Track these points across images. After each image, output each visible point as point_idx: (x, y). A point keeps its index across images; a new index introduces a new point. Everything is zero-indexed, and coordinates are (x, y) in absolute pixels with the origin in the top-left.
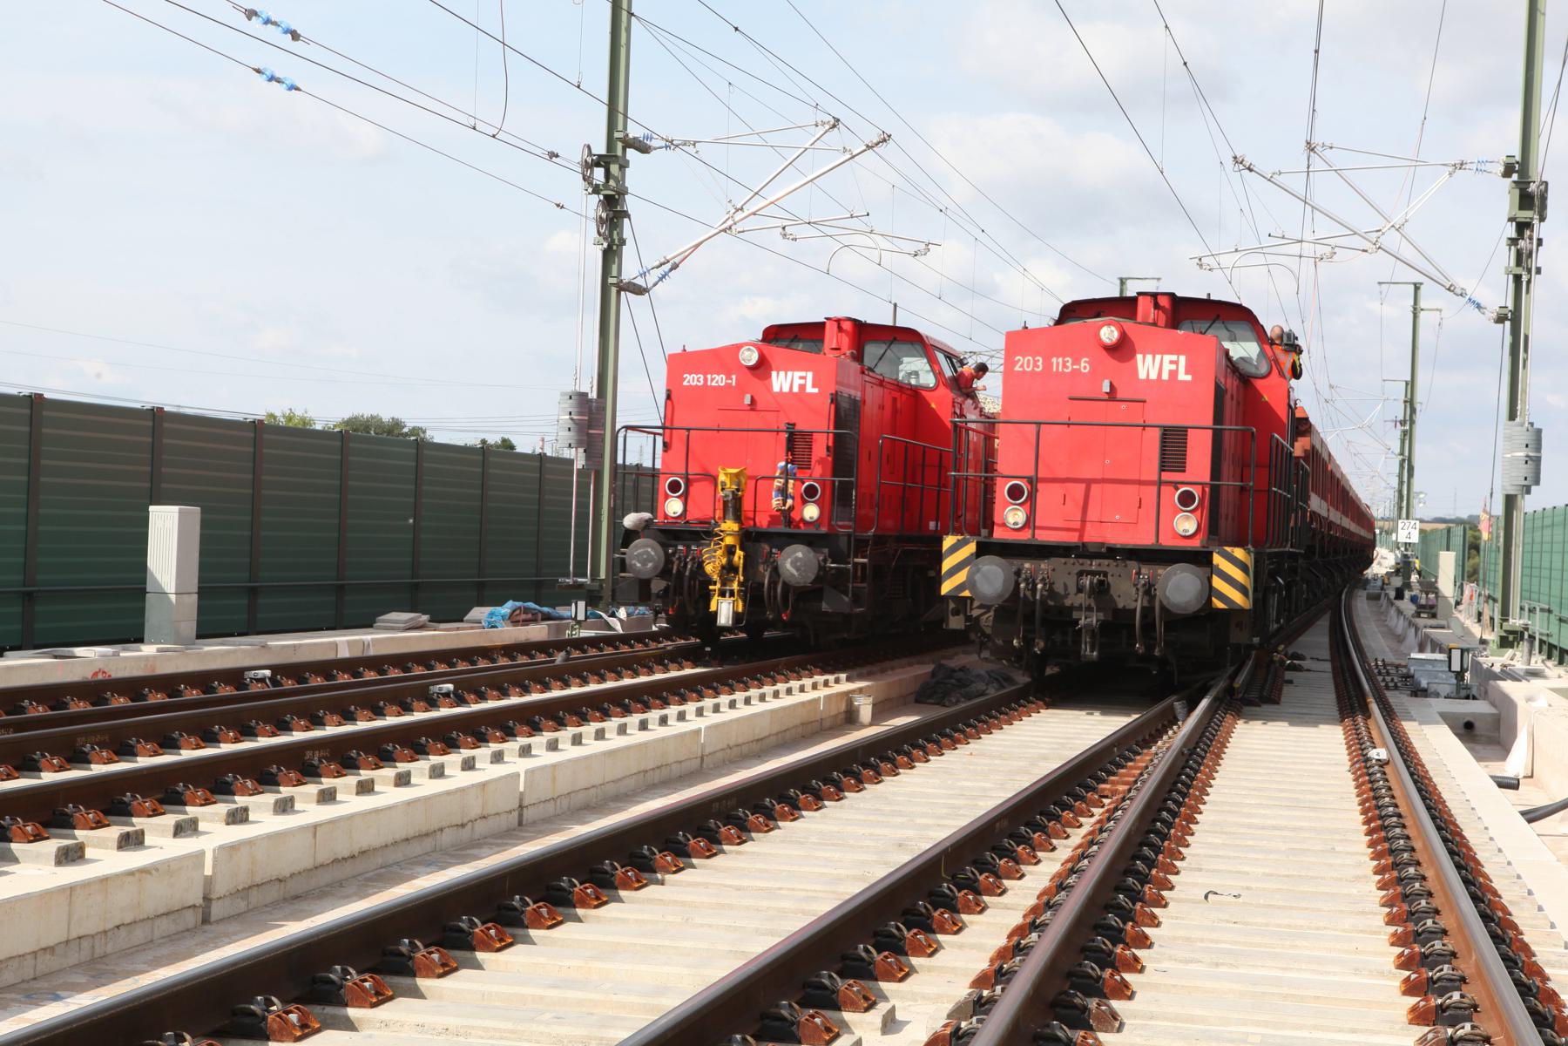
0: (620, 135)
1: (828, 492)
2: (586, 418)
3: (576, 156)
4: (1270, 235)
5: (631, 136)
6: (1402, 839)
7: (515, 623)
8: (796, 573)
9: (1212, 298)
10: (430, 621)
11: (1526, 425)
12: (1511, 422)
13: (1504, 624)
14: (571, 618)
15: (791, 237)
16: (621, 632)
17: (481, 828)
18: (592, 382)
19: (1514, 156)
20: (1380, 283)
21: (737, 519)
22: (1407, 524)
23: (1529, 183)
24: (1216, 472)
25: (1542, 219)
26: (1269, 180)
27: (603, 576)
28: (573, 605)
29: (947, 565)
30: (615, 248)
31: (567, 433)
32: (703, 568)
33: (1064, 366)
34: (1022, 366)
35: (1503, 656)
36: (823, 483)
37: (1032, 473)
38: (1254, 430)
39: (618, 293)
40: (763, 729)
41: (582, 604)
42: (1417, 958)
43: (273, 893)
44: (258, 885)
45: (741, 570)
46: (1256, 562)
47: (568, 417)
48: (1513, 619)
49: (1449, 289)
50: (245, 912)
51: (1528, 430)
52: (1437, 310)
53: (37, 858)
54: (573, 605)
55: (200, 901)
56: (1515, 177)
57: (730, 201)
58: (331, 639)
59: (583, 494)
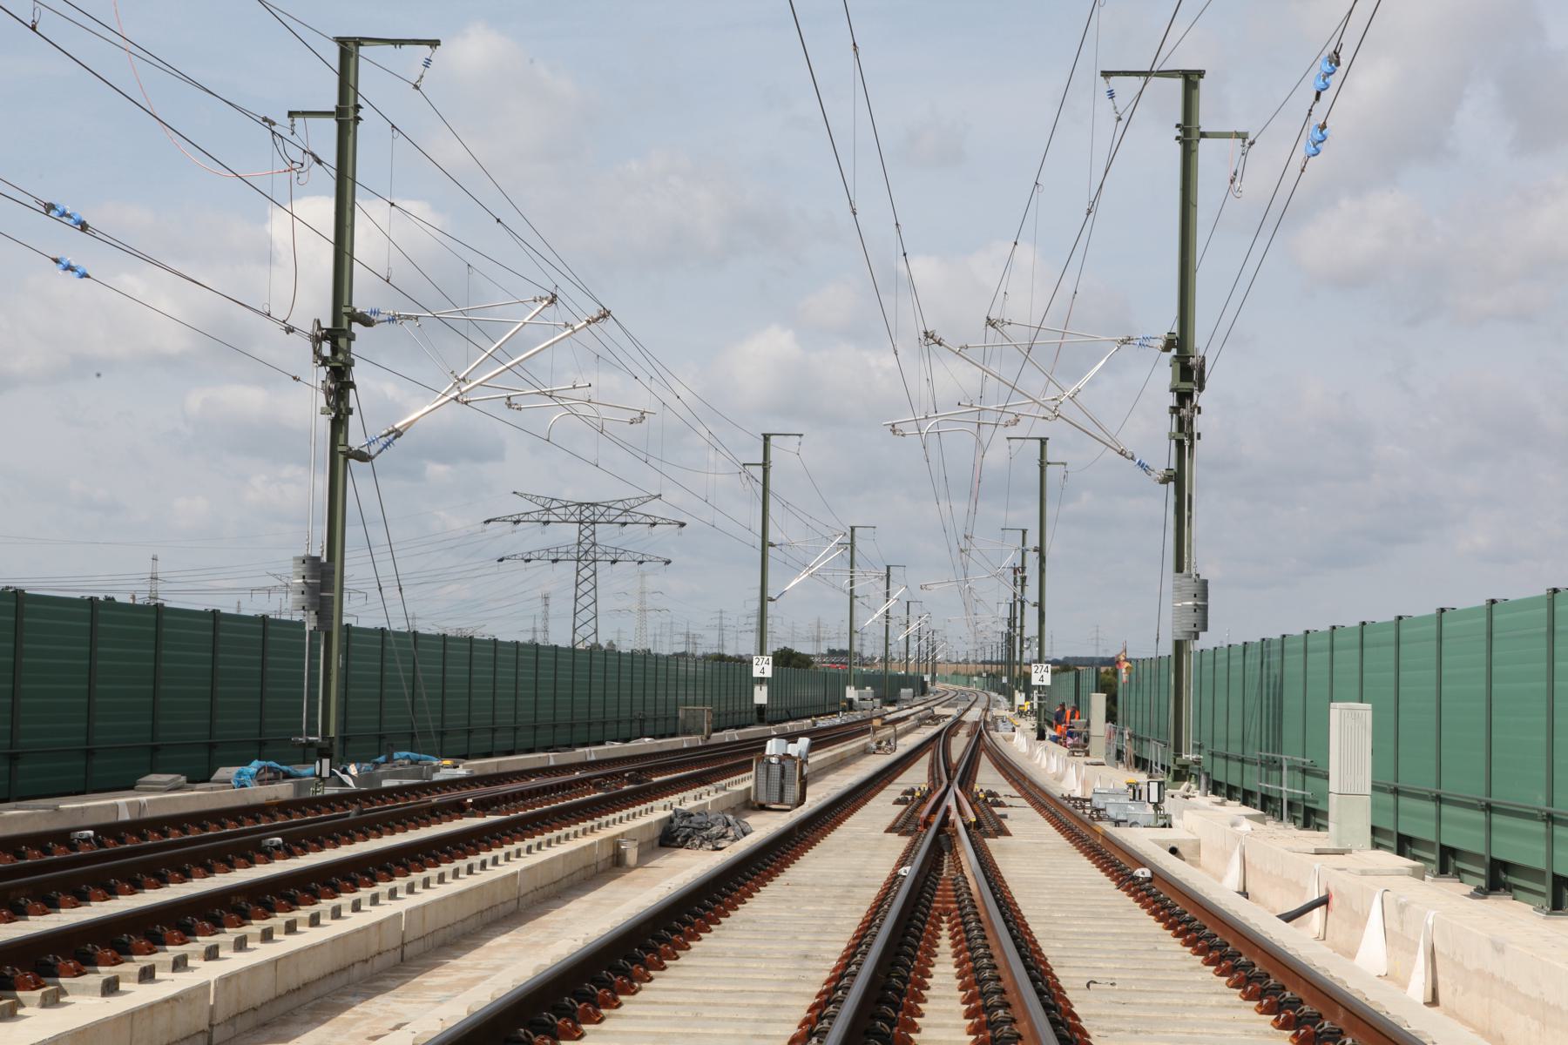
0: (348, 310)
2: (319, 581)
3: (309, 328)
4: (959, 404)
5: (358, 311)
6: (992, 980)
7: (261, 782)
10: (188, 782)
11: (1194, 576)
12: (1179, 574)
13: (1177, 759)
14: (315, 775)
15: (516, 407)
16: (355, 788)
17: (378, 963)
18: (323, 551)
19: (1174, 333)
20: (1008, 438)
22: (761, 660)
23: (1189, 357)
25: (1201, 388)
26: (957, 353)
27: (332, 734)
28: (318, 763)
30: (342, 417)
31: (301, 596)
35: (1179, 789)
39: (346, 461)
40: (559, 872)
41: (326, 762)
42: (1293, 1020)
43: (249, 1021)
44: (241, 1013)
47: (301, 581)
48: (1186, 754)
49: (1121, 453)
50: (233, 1037)
51: (1195, 581)
52: (1062, 463)
53: (85, 990)
54: (318, 763)
55: (206, 1027)
56: (1174, 351)
57: (452, 373)
58: (112, 801)
59: (314, 656)
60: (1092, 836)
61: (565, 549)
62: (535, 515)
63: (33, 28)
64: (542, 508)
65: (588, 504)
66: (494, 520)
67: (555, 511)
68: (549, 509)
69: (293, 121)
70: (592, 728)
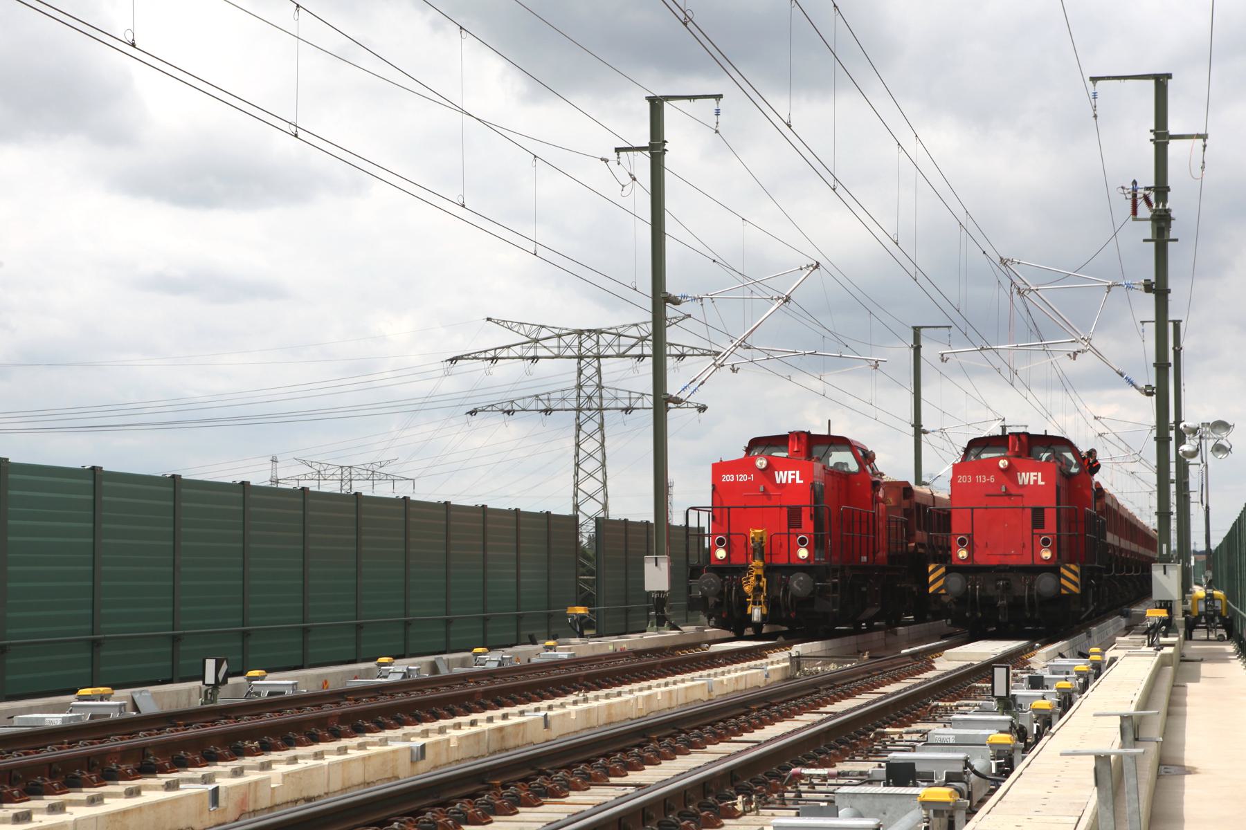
1: (813, 542)
8: (800, 589)
9: (1048, 434)
21: (762, 560)
24: (1059, 530)
29: (931, 579)
32: (743, 589)
33: (982, 479)
34: (961, 480)
36: (810, 537)
37: (970, 532)
38: (1076, 507)
45: (765, 588)
46: (1081, 571)
60: (1067, 365)
61: (559, 395)
62: (518, 351)
63: (535, 156)
64: (527, 339)
65: (589, 331)
66: (461, 358)
67: (545, 343)
68: (537, 341)
69: (618, 155)
70: (452, 628)
